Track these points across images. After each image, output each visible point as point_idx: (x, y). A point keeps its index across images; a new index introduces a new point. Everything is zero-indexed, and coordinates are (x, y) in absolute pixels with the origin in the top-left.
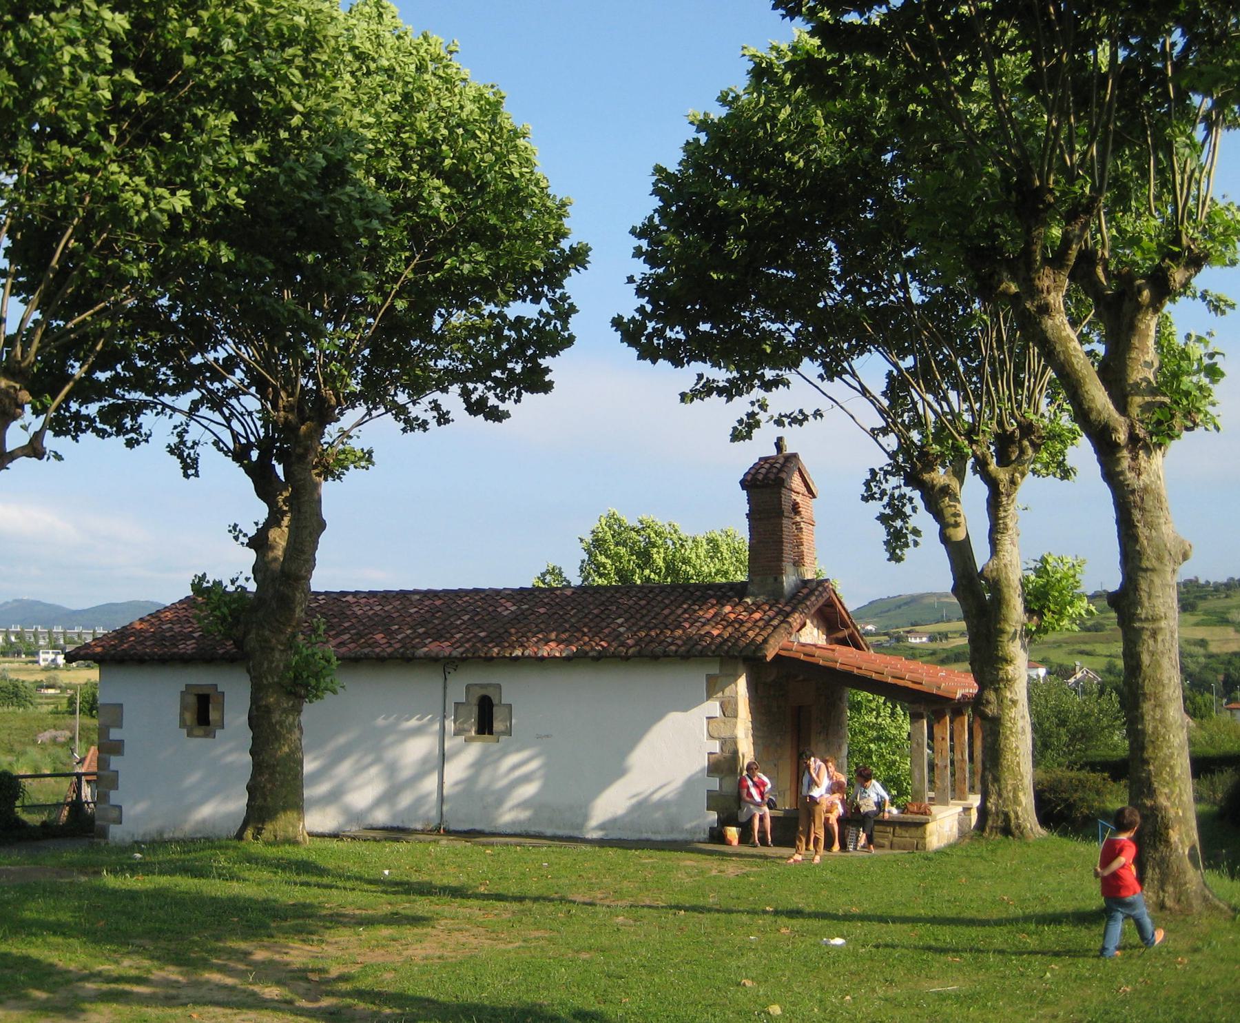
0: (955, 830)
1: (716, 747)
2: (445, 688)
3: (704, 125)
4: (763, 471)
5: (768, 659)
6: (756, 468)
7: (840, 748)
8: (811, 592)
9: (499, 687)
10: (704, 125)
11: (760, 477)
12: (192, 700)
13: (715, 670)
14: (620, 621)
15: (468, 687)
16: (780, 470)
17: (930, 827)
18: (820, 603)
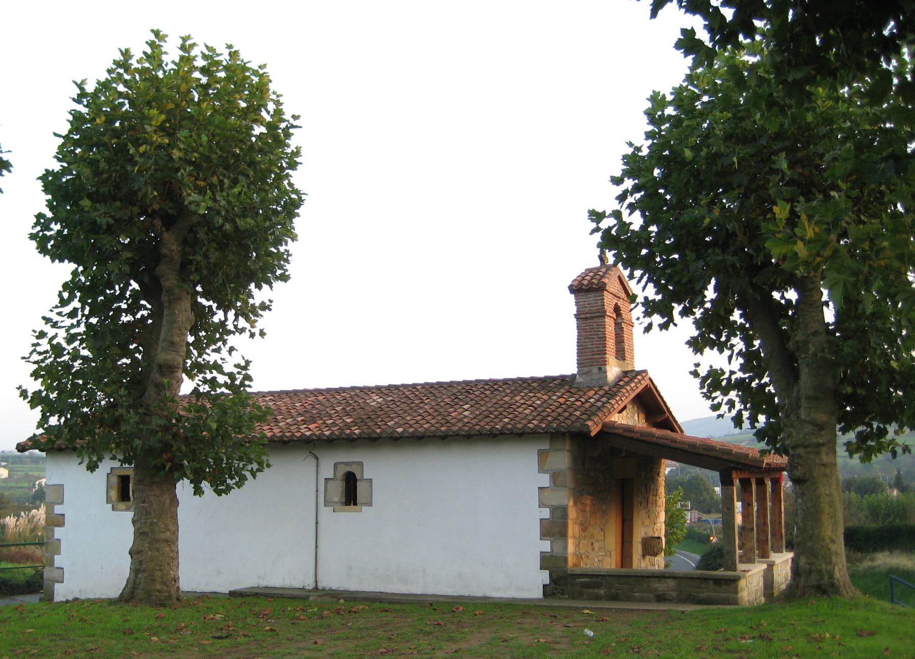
0: (761, 584)
1: (546, 513)
2: (317, 466)
3: (53, 261)
4: (588, 278)
5: (593, 434)
6: (582, 277)
7: (657, 516)
8: (631, 380)
9: (361, 464)
10: (53, 261)
11: (585, 282)
12: (115, 480)
13: (546, 446)
14: (466, 407)
15: (336, 465)
16: (602, 277)
17: (742, 583)
18: (637, 391)
